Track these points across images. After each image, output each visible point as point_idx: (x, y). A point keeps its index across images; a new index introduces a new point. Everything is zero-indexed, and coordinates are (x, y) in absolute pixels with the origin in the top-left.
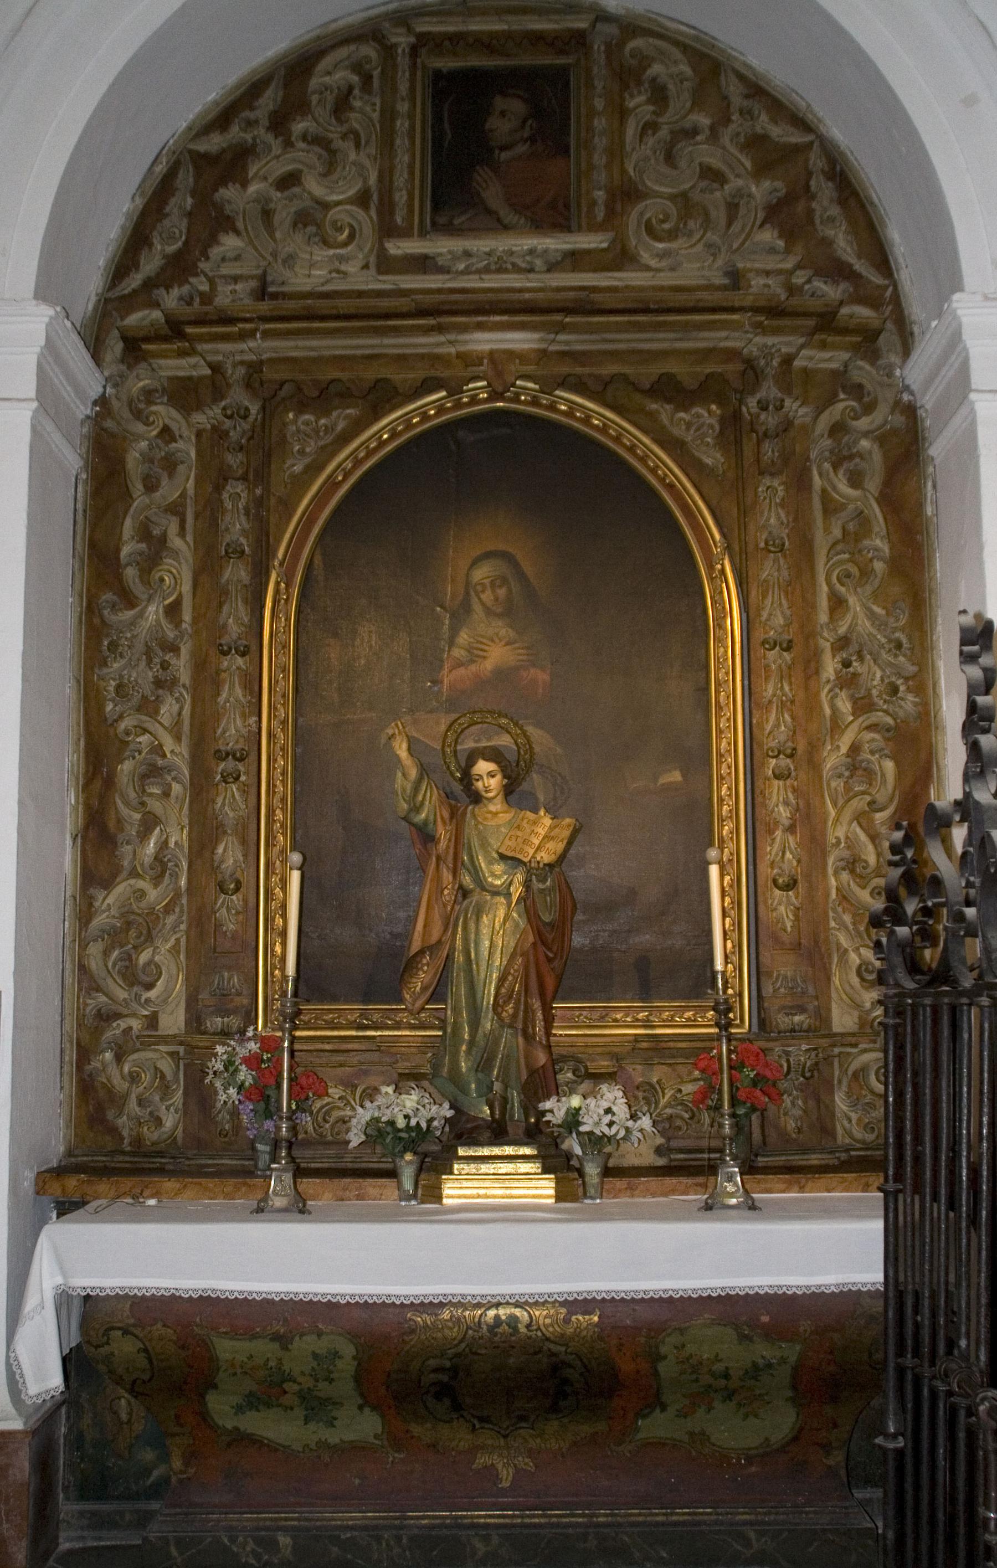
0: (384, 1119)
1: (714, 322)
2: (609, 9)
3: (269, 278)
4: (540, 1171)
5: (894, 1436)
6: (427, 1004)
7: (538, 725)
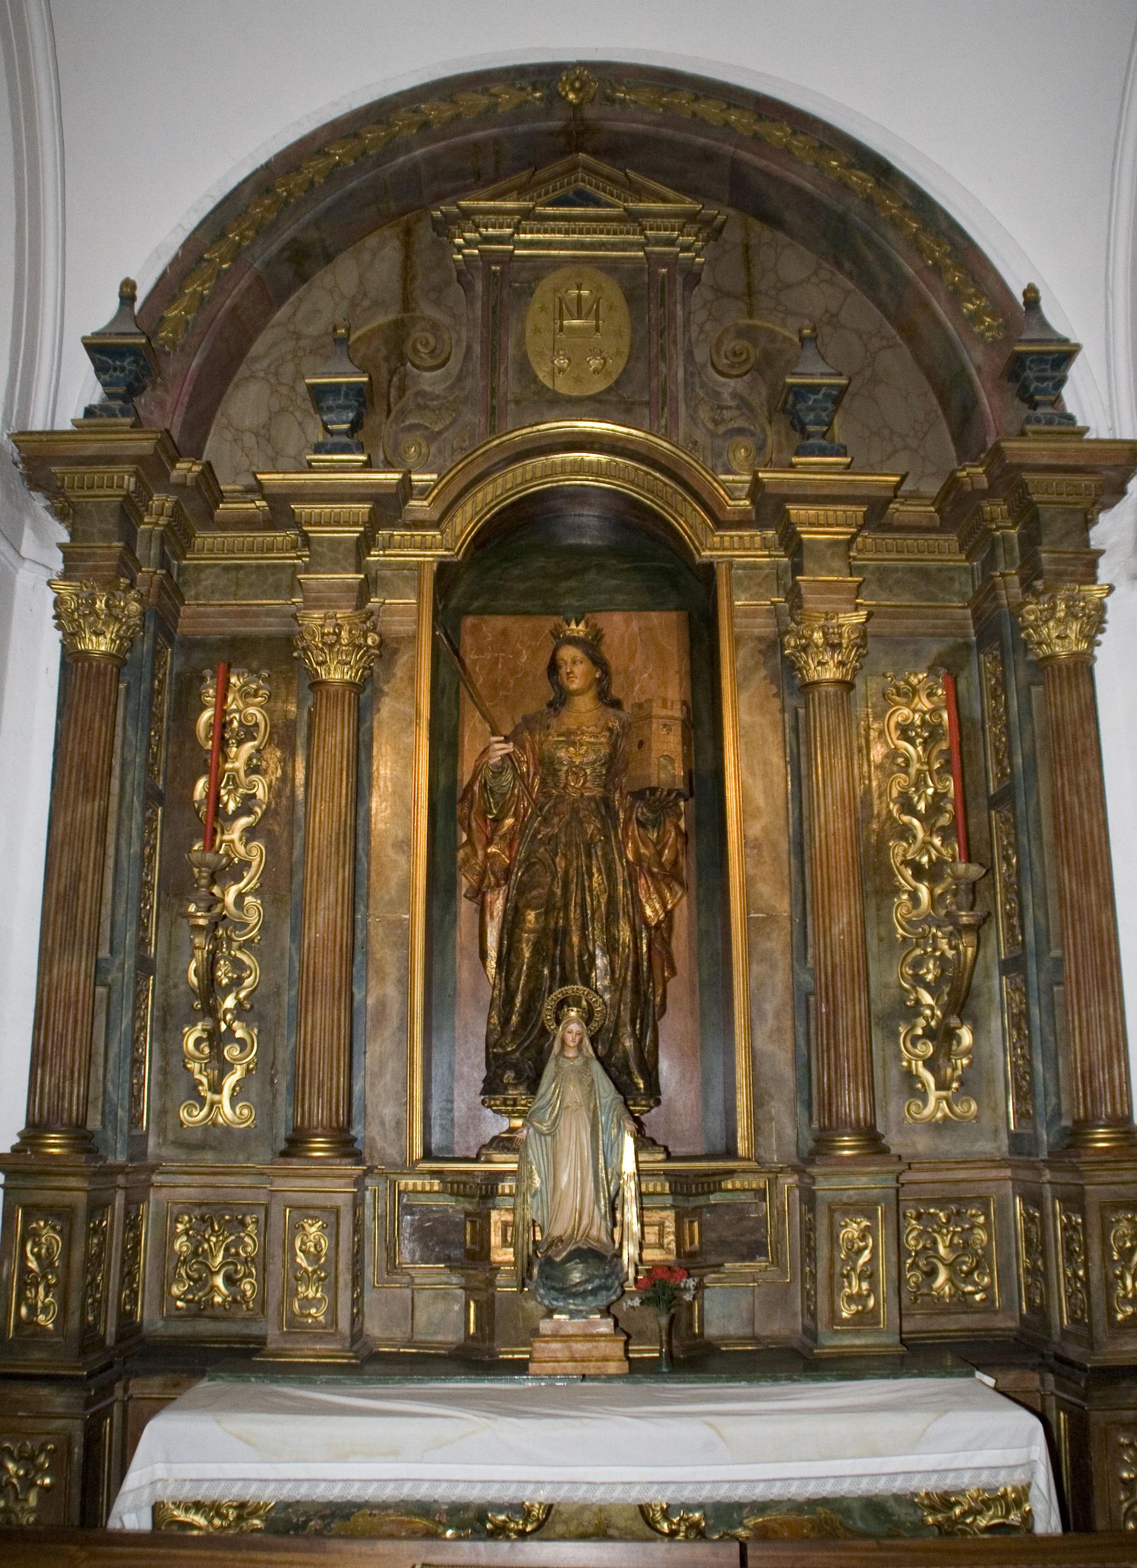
1: (23, 253)
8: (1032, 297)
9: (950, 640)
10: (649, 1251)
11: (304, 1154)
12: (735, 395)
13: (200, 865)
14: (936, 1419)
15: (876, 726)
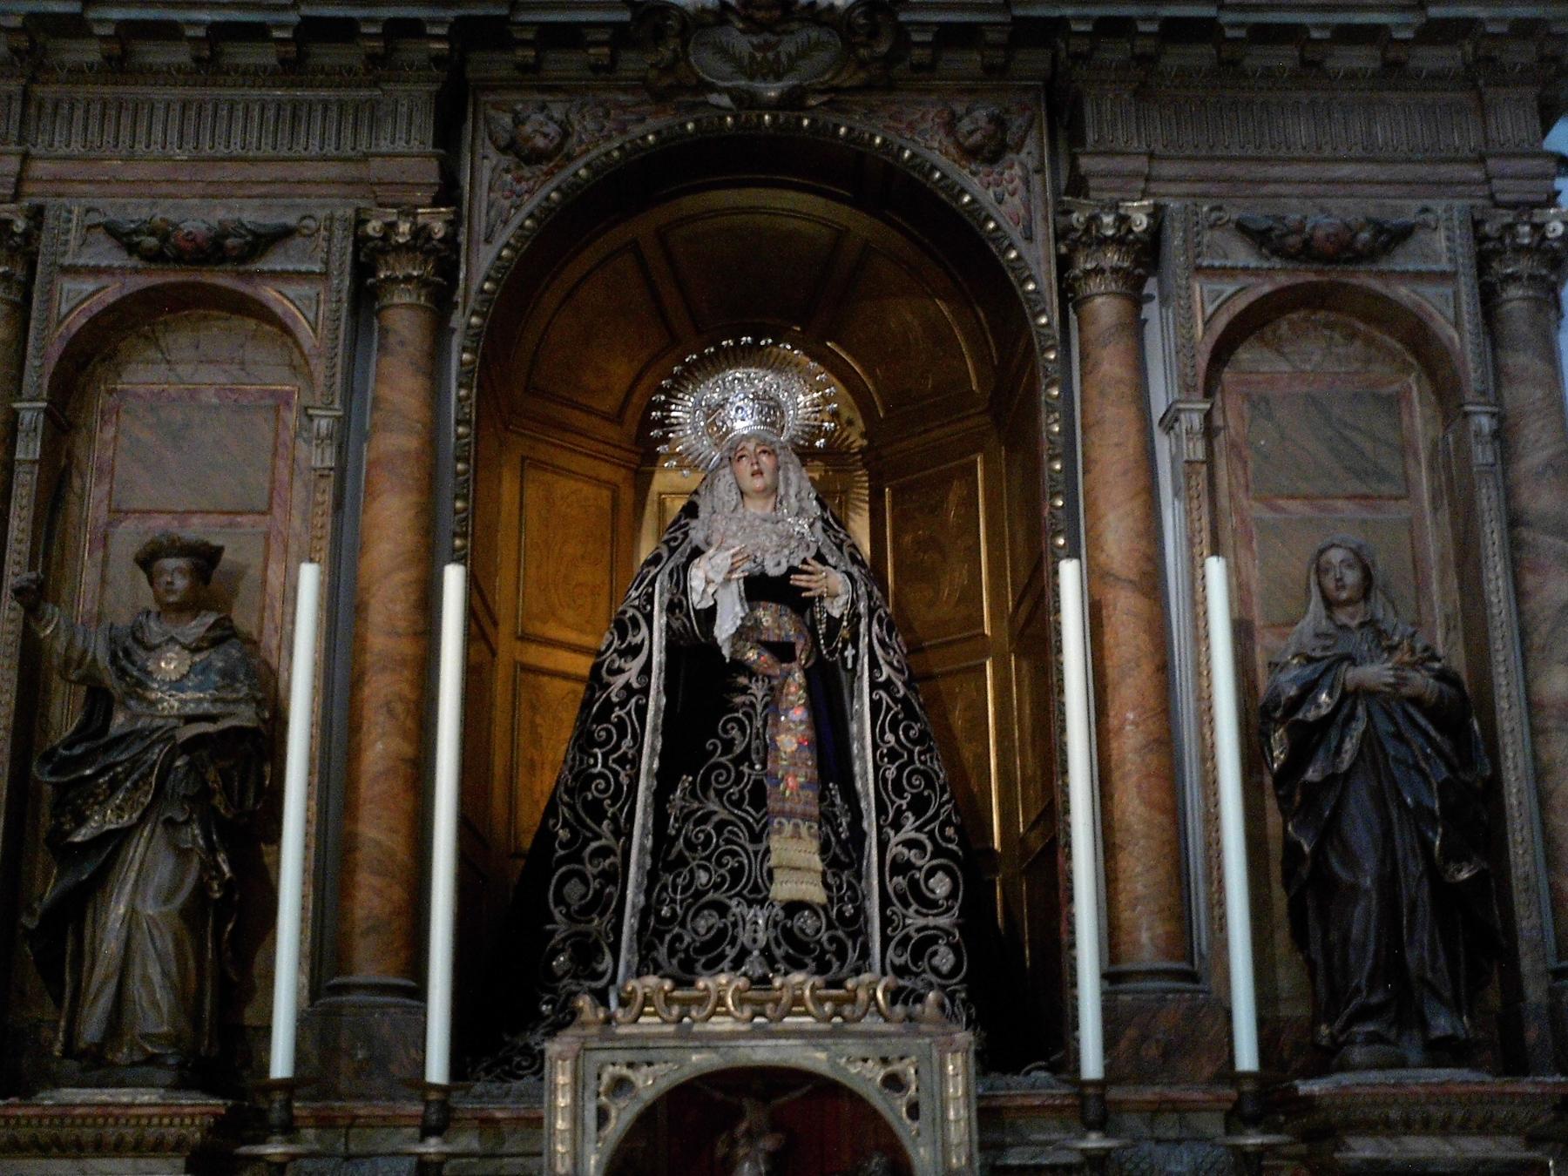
0: (384, 391)
2: (413, 597)
4: (429, 201)
6: (793, 1005)
8: (1146, 321)
9: (253, 267)
10: (40, 164)
12: (733, 947)
13: (969, 112)
15: (467, 410)
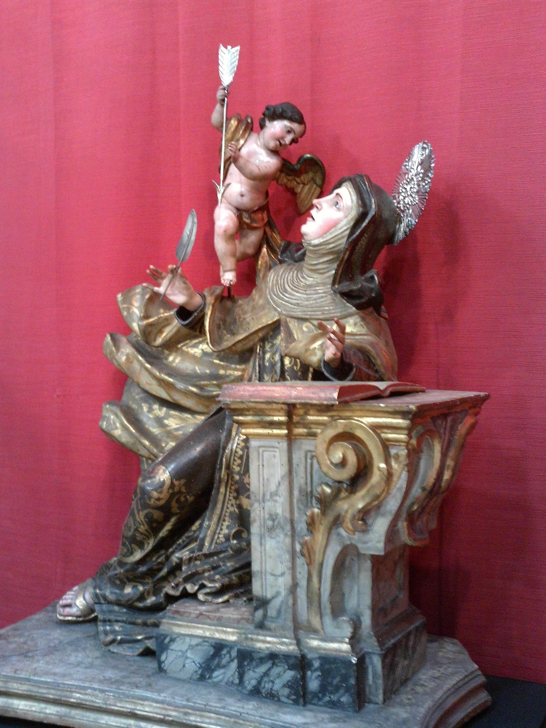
3: (284, 445)
5: (204, 297)
7: (182, 271)
11: (335, 256)
14: (264, 132)
